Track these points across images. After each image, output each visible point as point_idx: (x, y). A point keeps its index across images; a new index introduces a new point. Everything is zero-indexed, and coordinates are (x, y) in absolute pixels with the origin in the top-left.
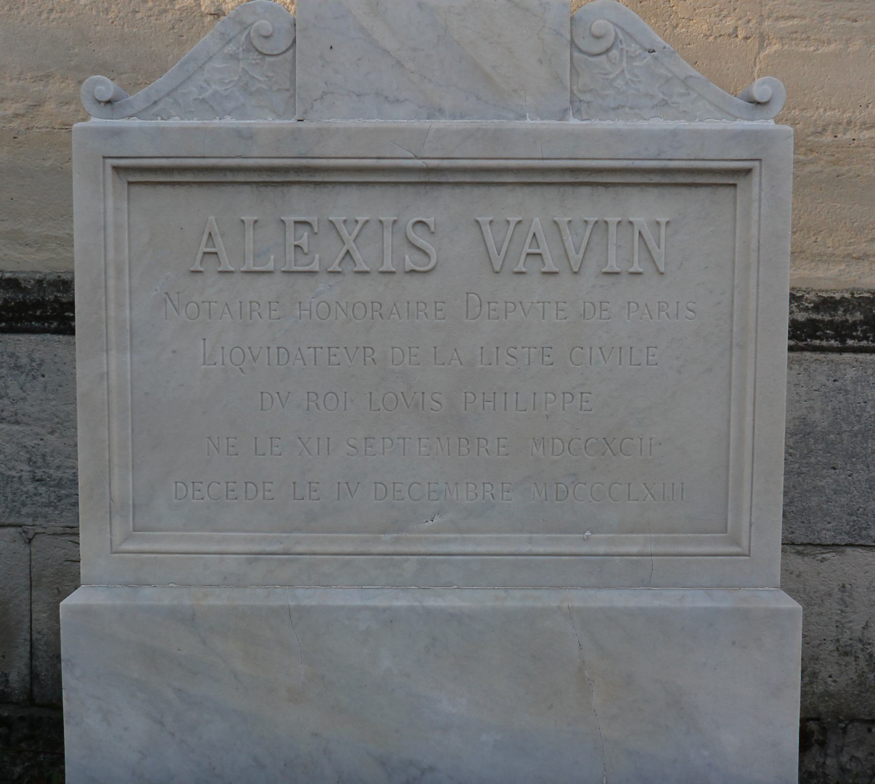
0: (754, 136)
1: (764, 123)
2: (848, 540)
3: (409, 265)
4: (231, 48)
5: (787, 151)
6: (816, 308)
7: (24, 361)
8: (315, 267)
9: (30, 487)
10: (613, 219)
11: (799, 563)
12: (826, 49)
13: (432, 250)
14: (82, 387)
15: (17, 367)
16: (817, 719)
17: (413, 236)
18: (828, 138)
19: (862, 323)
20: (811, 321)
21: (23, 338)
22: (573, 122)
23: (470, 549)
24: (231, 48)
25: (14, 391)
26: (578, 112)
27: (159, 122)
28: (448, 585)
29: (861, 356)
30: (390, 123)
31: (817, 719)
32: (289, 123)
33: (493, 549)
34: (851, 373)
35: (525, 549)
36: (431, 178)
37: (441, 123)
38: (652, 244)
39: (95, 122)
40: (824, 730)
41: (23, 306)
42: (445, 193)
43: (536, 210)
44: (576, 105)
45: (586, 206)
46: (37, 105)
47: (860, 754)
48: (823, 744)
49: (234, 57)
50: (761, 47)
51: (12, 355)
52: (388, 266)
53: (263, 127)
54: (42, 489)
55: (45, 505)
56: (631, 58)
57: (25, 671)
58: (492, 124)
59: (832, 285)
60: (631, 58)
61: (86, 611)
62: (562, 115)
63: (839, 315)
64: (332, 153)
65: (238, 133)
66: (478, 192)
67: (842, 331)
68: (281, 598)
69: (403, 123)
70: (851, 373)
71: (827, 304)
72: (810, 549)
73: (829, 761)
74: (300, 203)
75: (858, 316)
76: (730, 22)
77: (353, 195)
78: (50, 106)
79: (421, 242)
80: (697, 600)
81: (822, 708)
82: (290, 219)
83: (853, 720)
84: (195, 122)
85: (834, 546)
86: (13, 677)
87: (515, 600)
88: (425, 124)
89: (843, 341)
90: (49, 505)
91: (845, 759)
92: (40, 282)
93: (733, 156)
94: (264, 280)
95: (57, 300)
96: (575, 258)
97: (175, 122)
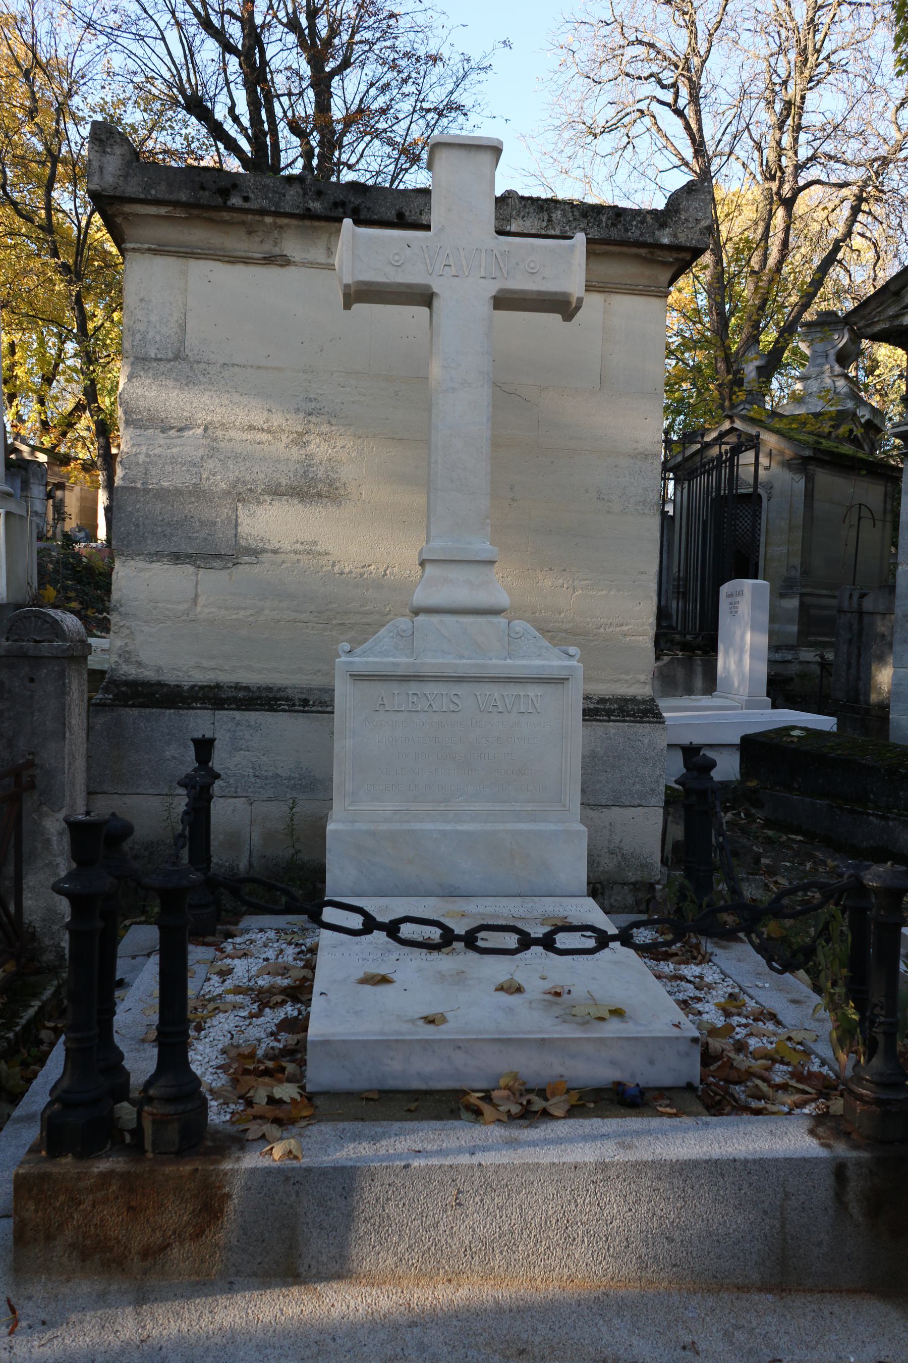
0: (570, 667)
1: (574, 663)
2: (612, 803)
3: (452, 709)
4: (391, 634)
5: (580, 673)
6: (598, 703)
7: (253, 723)
8: (419, 709)
9: (253, 780)
10: (522, 694)
11: (591, 813)
12: (600, 593)
13: (459, 703)
14: (336, 751)
15: (249, 726)
16: (600, 883)
17: (453, 699)
18: (602, 630)
19: (618, 709)
20: (596, 708)
21: (252, 713)
22: (509, 661)
23: (472, 808)
24: (391, 634)
25: (247, 737)
26: (510, 658)
27: (365, 659)
28: (464, 822)
29: (617, 724)
30: (446, 661)
31: (600, 883)
32: (411, 660)
33: (480, 809)
34: (613, 731)
35: (492, 808)
36: (460, 680)
37: (464, 661)
38: (535, 703)
39: (343, 659)
40: (603, 888)
41: (251, 699)
42: (465, 684)
43: (496, 691)
44: (510, 656)
45: (513, 690)
46: (262, 610)
47: (619, 898)
48: (603, 894)
49: (392, 637)
50: (574, 592)
51: (247, 721)
52: (444, 709)
53: (402, 661)
54: (258, 781)
55: (261, 787)
56: (528, 640)
57: (247, 863)
58: (481, 662)
59: (604, 693)
60: (528, 640)
61: (336, 832)
62: (505, 659)
63: (608, 706)
64: (426, 671)
65: (394, 664)
66: (476, 684)
67: (609, 712)
68: (406, 826)
69: (451, 661)
70: (613, 731)
71: (602, 701)
72: (596, 807)
73: (606, 902)
74: (414, 687)
75: (616, 706)
76: (561, 581)
77: (432, 684)
78: (266, 612)
79: (456, 701)
80: (552, 827)
81: (602, 878)
82: (410, 692)
83: (615, 883)
84: (378, 659)
85: (607, 806)
86: (241, 866)
87: (488, 827)
88: (458, 661)
89: (609, 717)
90: (261, 787)
91: (612, 901)
92: (259, 688)
93: (563, 674)
94: (400, 714)
95: (267, 696)
96: (509, 707)
97: (371, 659)
